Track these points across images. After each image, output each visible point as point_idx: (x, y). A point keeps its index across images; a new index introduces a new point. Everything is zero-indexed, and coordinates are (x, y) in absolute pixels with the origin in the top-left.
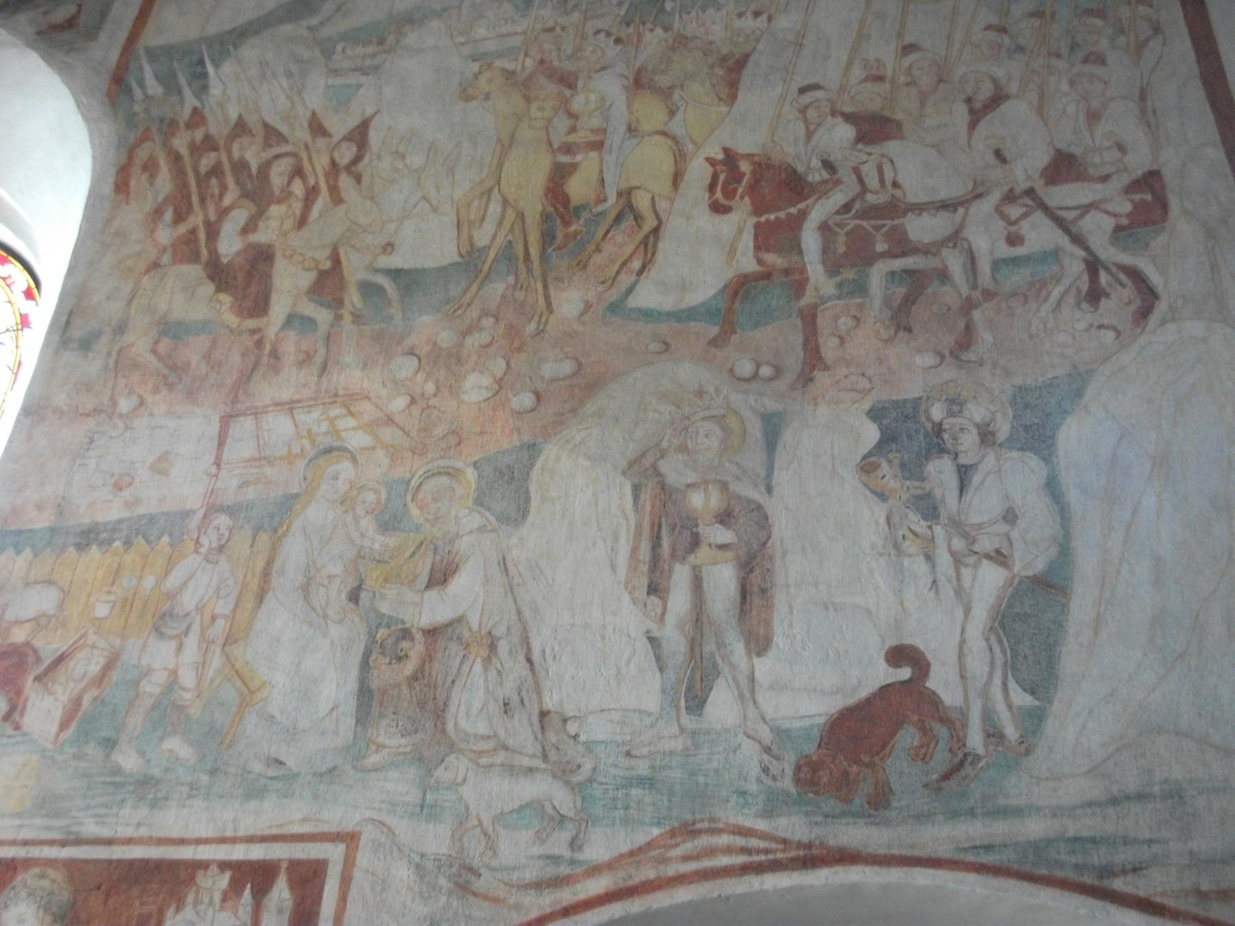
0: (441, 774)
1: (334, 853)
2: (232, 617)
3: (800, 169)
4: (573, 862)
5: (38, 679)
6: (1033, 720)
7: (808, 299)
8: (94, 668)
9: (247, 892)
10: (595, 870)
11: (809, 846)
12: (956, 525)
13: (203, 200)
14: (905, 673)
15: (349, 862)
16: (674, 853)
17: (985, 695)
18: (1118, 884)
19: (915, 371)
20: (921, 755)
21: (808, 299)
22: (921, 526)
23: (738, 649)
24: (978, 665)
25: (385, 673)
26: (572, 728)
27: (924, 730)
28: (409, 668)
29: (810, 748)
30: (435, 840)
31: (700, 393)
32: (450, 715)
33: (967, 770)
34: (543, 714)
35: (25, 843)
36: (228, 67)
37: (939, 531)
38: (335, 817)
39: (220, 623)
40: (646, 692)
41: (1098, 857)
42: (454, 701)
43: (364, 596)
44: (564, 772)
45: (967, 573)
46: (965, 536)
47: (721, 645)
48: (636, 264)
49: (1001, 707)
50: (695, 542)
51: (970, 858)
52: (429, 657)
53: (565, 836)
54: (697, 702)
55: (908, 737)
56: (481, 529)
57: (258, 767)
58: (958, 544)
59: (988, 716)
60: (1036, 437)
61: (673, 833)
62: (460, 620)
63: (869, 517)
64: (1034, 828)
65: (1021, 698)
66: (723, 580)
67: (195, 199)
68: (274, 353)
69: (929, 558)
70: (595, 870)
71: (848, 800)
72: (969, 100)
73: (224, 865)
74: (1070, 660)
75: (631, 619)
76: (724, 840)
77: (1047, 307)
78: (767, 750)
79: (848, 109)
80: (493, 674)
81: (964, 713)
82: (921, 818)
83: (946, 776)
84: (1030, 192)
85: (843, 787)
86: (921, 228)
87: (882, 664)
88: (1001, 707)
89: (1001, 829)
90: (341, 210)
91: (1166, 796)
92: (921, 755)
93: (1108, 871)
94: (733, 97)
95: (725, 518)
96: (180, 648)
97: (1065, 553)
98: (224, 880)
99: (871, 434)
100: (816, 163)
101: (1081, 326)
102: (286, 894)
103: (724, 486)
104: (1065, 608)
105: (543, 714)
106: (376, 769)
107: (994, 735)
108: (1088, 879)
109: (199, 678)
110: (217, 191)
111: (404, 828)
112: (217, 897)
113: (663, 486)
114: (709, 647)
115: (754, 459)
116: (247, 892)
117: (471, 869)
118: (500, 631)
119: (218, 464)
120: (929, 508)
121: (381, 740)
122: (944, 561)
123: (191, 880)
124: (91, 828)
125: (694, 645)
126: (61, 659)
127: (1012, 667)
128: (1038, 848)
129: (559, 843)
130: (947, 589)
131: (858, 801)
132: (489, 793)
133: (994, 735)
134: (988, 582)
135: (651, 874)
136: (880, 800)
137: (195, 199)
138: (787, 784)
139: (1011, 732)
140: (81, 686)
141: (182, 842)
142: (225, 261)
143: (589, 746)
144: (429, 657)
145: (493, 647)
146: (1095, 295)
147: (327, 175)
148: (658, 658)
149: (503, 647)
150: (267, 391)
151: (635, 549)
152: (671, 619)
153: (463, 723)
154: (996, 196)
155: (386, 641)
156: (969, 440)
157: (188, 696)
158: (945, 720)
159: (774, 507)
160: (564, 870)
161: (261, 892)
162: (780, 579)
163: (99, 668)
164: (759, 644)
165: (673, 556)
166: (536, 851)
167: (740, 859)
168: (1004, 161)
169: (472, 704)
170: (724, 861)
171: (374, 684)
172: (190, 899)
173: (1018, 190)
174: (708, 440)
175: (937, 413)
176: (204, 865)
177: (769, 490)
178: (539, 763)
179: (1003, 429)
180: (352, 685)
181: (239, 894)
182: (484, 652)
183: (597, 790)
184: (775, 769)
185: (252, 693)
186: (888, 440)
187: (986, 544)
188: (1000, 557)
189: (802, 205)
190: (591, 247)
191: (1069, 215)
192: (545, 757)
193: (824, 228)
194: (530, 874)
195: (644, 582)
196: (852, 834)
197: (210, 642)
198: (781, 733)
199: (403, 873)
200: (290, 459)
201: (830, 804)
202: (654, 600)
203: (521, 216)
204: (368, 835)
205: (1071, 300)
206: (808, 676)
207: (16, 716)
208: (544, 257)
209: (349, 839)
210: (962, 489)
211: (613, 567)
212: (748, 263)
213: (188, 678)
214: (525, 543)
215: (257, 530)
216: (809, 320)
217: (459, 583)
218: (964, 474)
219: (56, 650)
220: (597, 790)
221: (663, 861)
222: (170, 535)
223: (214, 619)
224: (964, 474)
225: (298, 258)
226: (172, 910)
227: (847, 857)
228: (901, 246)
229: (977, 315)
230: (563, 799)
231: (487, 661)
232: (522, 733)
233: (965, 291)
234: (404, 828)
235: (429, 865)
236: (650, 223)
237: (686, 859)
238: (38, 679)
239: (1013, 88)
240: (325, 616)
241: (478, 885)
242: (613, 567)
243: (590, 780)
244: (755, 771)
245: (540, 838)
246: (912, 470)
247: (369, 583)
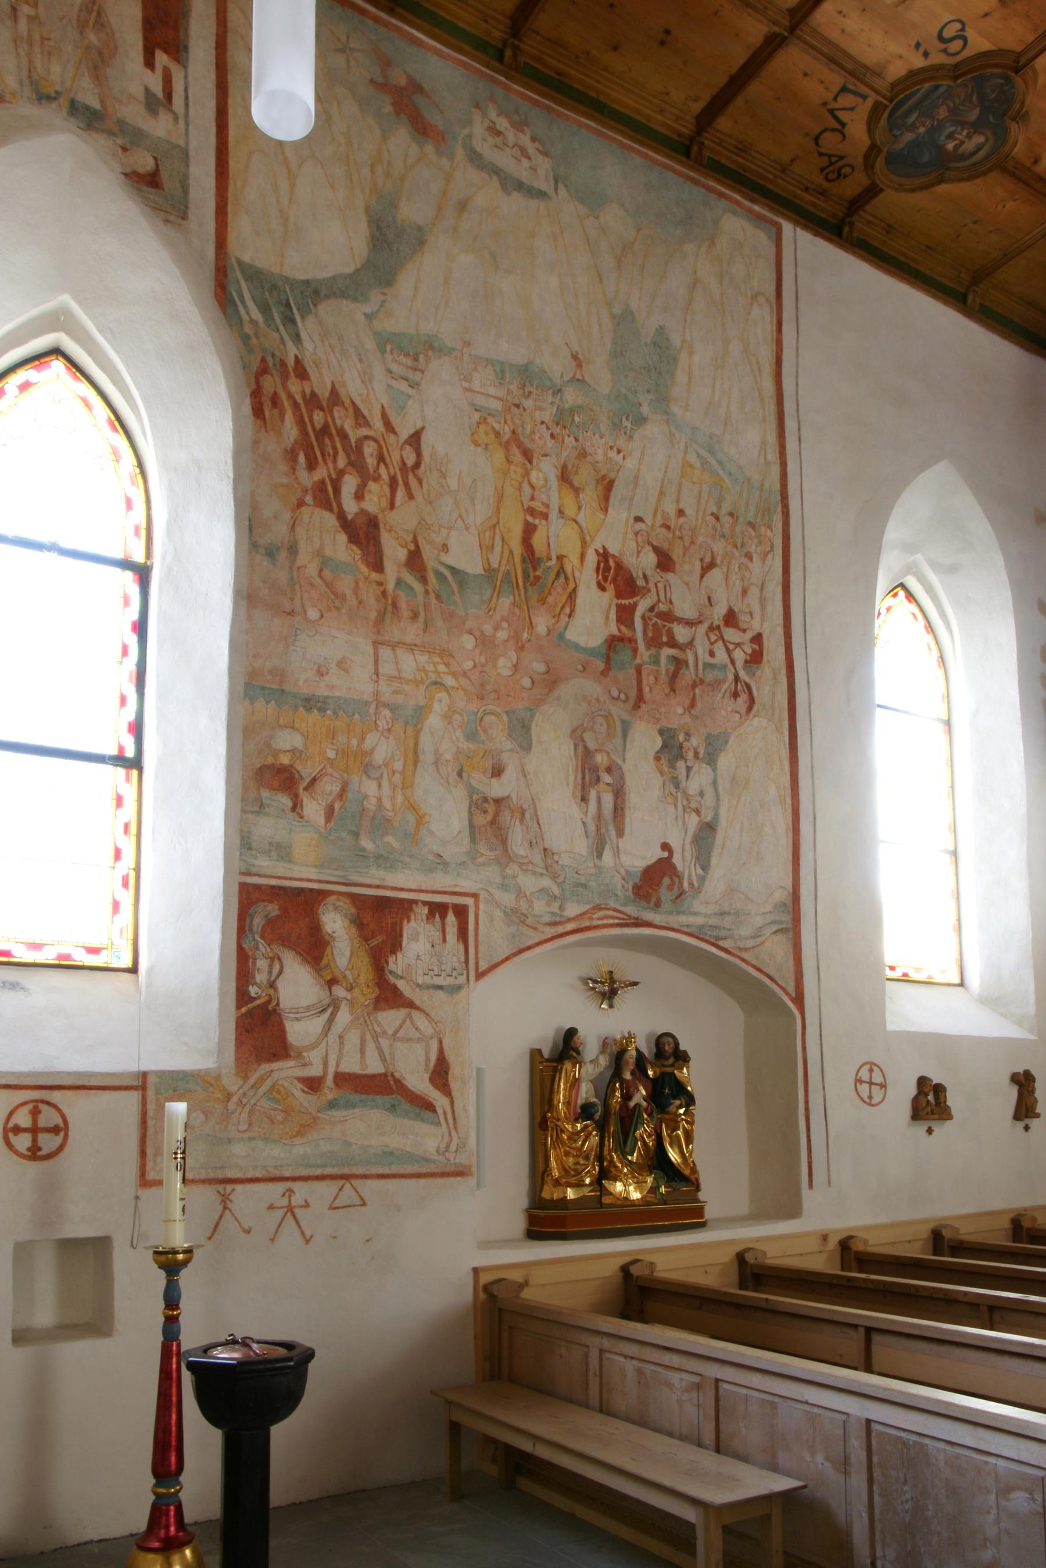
0: (509, 871)
1: (469, 901)
2: (403, 773)
3: (634, 575)
4: (561, 916)
5: (306, 789)
6: (702, 879)
7: (638, 661)
8: (336, 788)
9: (437, 916)
10: (569, 920)
11: (637, 919)
12: (685, 794)
13: (323, 456)
14: (666, 854)
15: (477, 907)
16: (596, 916)
17: (689, 868)
18: (720, 943)
19: (676, 715)
20: (670, 888)
21: (638, 661)
22: (673, 791)
23: (613, 833)
24: (688, 856)
25: (481, 820)
26: (556, 858)
27: (672, 879)
28: (489, 817)
29: (637, 880)
30: (508, 899)
31: (598, 700)
32: (509, 844)
33: (683, 896)
34: (545, 850)
35: (320, 882)
36: (311, 319)
37: (679, 795)
38: (466, 884)
39: (397, 775)
40: (582, 846)
41: (716, 933)
42: (510, 838)
43: (464, 775)
44: (554, 877)
45: (687, 815)
46: (687, 799)
47: (607, 831)
48: (567, 610)
49: (693, 874)
50: (598, 780)
51: (686, 930)
52: (497, 814)
53: (557, 904)
54: (600, 855)
55: (666, 881)
56: (512, 750)
57: (431, 857)
58: (685, 802)
59: (690, 876)
60: (711, 760)
61: (594, 908)
62: (508, 797)
63: (657, 781)
64: (700, 920)
65: (700, 872)
66: (608, 800)
67: (320, 459)
68: (394, 605)
69: (676, 806)
70: (569, 920)
71: (649, 902)
72: (702, 560)
73: (425, 903)
74: (714, 861)
75: (575, 811)
76: (611, 913)
77: (720, 695)
78: (624, 879)
79: (655, 543)
80: (525, 828)
81: (683, 873)
82: (670, 913)
83: (677, 898)
84: (718, 627)
85: (647, 898)
86: (681, 633)
87: (659, 849)
88: (693, 874)
89: (691, 919)
90: (413, 503)
91: (735, 914)
92: (670, 888)
93: (718, 938)
94: (606, 510)
95: (609, 770)
96: (380, 786)
97: (716, 816)
98: (426, 910)
99: (659, 743)
100: (641, 574)
101: (730, 709)
102: (453, 919)
103: (608, 754)
104: (714, 837)
105: (545, 850)
106: (482, 865)
107: (691, 884)
108: (712, 940)
109: (394, 805)
110: (331, 452)
111: (498, 894)
112: (424, 917)
113: (586, 748)
114: (603, 831)
115: (618, 741)
116: (437, 916)
117: (525, 915)
118: (525, 807)
119: (377, 674)
120: (676, 783)
121: (482, 851)
122: (680, 808)
123: (411, 909)
124: (355, 878)
125: (598, 829)
126: (314, 780)
127: (697, 858)
128: (701, 927)
129: (555, 907)
130: (680, 821)
131: (652, 904)
132: (529, 883)
133: (691, 884)
134: (693, 820)
135: (587, 923)
136: (658, 904)
137: (320, 459)
138: (630, 893)
139: (695, 883)
140: (331, 798)
141: (402, 890)
142: (350, 517)
143: (563, 866)
144: (497, 814)
145: (523, 814)
146: (736, 695)
147: (400, 470)
148: (586, 832)
149: (527, 815)
150: (394, 631)
151: (576, 778)
152: (589, 814)
153: (514, 848)
154: (706, 625)
155: (479, 803)
156: (690, 754)
157: (390, 814)
158: (678, 877)
159: (626, 768)
160: (558, 919)
161: (443, 917)
162: (627, 804)
163: (338, 789)
164: (620, 833)
165: (590, 784)
166: (547, 910)
167: (616, 921)
168: (711, 605)
169: (518, 840)
170: (611, 921)
171: (476, 823)
172: (412, 917)
173: (715, 625)
174: (601, 727)
175: (681, 737)
176: (416, 902)
177: (624, 760)
178: (544, 872)
179: (702, 752)
180: (466, 823)
181: (434, 916)
182: (520, 816)
183: (567, 886)
184: (626, 886)
185: (421, 818)
186: (665, 746)
187: (693, 805)
188: (697, 811)
189: (635, 599)
190: (547, 591)
191: (731, 647)
192: (547, 869)
193: (643, 617)
194: (547, 919)
195: (579, 794)
196: (649, 916)
197: (395, 786)
198: (628, 872)
199: (498, 914)
200: (417, 683)
201: (643, 904)
202: (583, 804)
203: (511, 552)
204: (483, 895)
205: (728, 695)
206: (637, 852)
207: (298, 809)
208: (525, 588)
209: (475, 896)
210: (688, 777)
211: (568, 784)
212: (613, 629)
213: (387, 803)
214: (533, 760)
215: (406, 723)
216: (639, 670)
217: (506, 776)
218: (689, 769)
219: (311, 774)
220: (567, 886)
221: (591, 919)
222: (360, 714)
223: (394, 772)
224: (689, 769)
225: (393, 534)
226: (405, 922)
227: (649, 925)
228: (673, 643)
229: (697, 691)
230: (556, 890)
231: (522, 820)
232: (538, 858)
233: (694, 676)
234: (498, 894)
235: (508, 911)
236: (572, 586)
237: (599, 919)
238: (306, 789)
239: (718, 561)
240: (448, 783)
241: (527, 921)
242: (568, 784)
243: (564, 882)
244: (619, 887)
245: (548, 904)
246: (672, 765)
247: (465, 769)
